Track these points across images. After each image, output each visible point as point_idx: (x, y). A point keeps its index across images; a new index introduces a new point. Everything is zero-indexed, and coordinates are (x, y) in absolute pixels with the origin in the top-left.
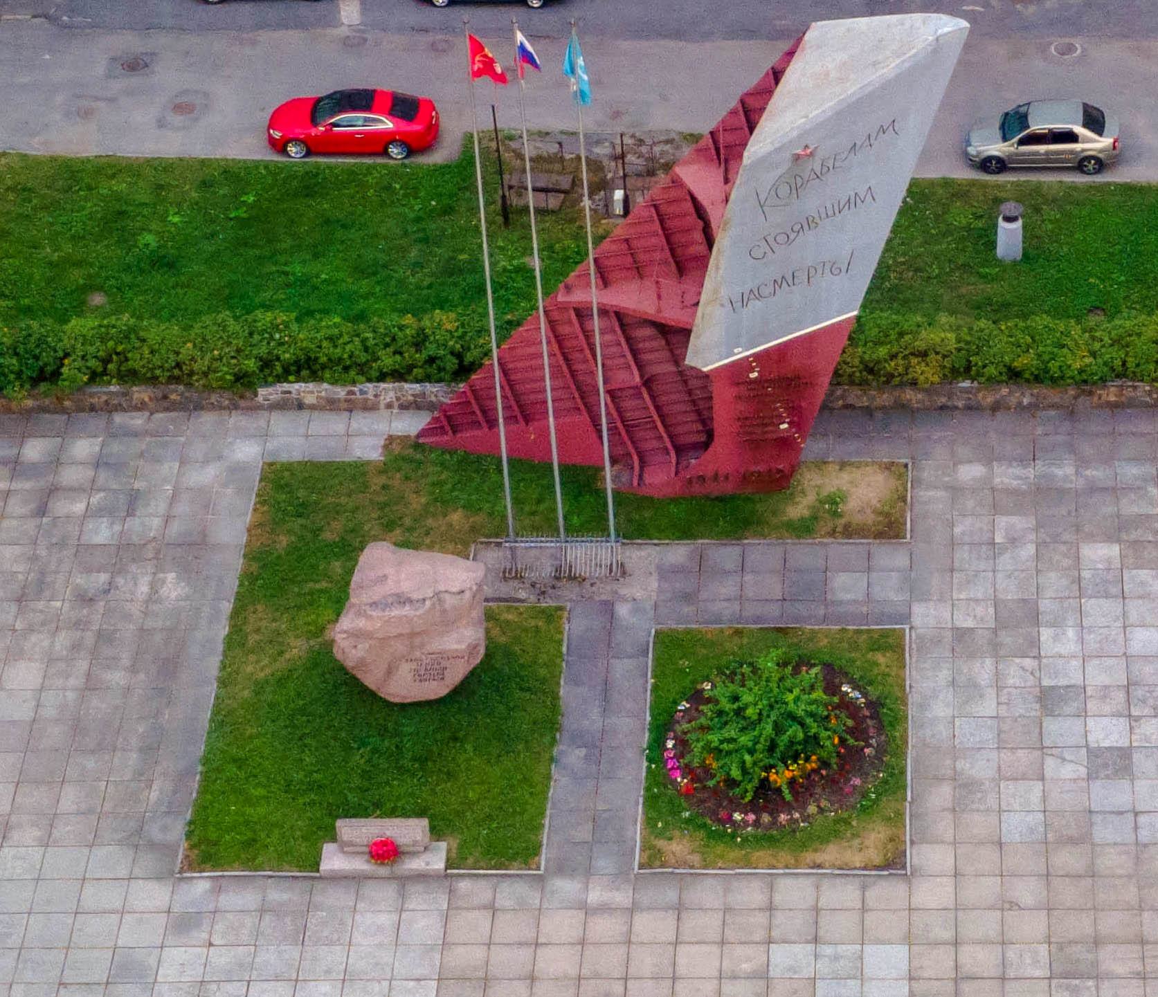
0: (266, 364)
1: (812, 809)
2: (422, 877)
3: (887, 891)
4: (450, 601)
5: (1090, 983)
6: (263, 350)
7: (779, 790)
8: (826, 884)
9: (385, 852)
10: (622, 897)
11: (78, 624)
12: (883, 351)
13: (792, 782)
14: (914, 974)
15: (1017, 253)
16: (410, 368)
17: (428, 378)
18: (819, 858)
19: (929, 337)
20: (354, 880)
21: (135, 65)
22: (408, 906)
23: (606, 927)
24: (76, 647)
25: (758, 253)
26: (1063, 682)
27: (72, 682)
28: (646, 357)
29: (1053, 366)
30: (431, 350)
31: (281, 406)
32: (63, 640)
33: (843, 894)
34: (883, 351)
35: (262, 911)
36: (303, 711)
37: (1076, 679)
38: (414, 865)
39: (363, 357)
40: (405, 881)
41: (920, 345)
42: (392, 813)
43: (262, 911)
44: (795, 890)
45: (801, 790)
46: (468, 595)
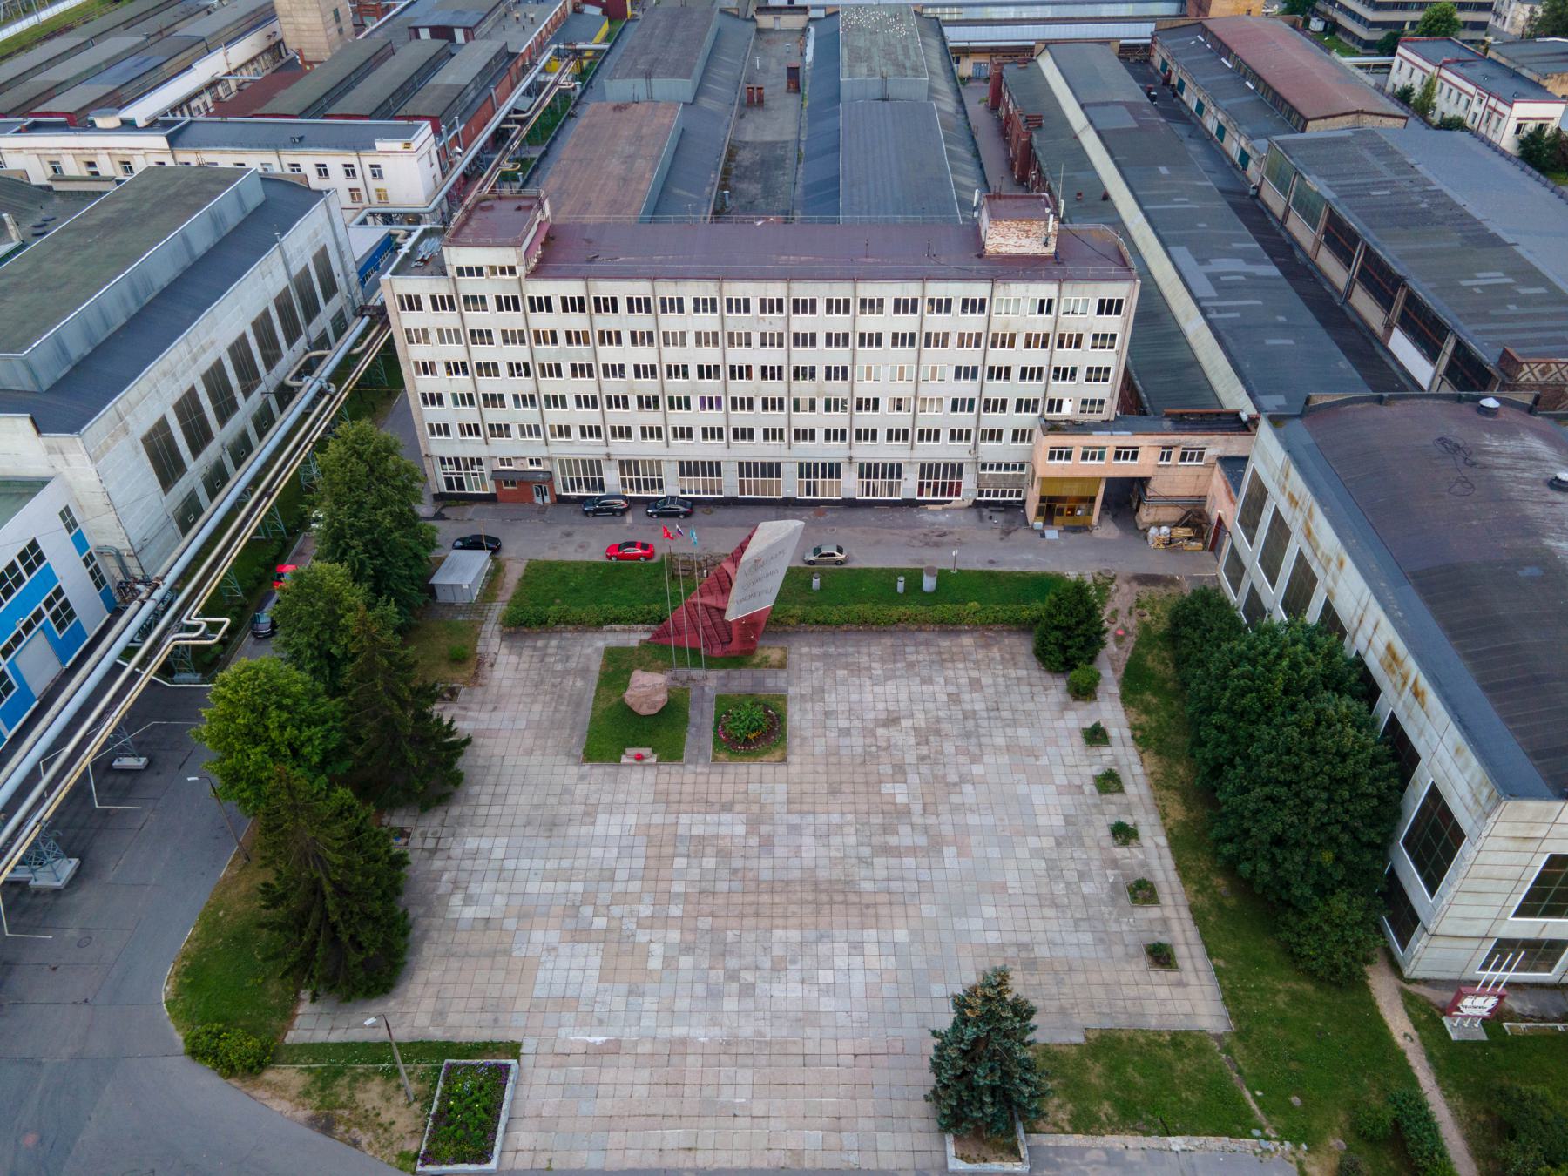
3: (781, 769)
9: (639, 758)
10: (706, 770)
19: (793, 611)
20: (631, 765)
21: (569, 534)
23: (702, 779)
33: (769, 769)
44: (755, 768)
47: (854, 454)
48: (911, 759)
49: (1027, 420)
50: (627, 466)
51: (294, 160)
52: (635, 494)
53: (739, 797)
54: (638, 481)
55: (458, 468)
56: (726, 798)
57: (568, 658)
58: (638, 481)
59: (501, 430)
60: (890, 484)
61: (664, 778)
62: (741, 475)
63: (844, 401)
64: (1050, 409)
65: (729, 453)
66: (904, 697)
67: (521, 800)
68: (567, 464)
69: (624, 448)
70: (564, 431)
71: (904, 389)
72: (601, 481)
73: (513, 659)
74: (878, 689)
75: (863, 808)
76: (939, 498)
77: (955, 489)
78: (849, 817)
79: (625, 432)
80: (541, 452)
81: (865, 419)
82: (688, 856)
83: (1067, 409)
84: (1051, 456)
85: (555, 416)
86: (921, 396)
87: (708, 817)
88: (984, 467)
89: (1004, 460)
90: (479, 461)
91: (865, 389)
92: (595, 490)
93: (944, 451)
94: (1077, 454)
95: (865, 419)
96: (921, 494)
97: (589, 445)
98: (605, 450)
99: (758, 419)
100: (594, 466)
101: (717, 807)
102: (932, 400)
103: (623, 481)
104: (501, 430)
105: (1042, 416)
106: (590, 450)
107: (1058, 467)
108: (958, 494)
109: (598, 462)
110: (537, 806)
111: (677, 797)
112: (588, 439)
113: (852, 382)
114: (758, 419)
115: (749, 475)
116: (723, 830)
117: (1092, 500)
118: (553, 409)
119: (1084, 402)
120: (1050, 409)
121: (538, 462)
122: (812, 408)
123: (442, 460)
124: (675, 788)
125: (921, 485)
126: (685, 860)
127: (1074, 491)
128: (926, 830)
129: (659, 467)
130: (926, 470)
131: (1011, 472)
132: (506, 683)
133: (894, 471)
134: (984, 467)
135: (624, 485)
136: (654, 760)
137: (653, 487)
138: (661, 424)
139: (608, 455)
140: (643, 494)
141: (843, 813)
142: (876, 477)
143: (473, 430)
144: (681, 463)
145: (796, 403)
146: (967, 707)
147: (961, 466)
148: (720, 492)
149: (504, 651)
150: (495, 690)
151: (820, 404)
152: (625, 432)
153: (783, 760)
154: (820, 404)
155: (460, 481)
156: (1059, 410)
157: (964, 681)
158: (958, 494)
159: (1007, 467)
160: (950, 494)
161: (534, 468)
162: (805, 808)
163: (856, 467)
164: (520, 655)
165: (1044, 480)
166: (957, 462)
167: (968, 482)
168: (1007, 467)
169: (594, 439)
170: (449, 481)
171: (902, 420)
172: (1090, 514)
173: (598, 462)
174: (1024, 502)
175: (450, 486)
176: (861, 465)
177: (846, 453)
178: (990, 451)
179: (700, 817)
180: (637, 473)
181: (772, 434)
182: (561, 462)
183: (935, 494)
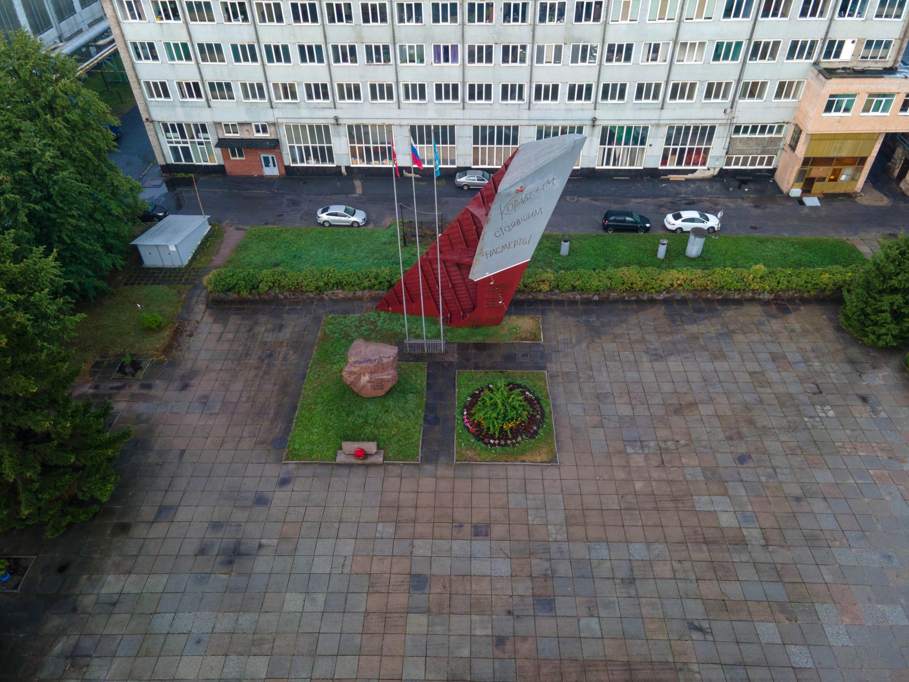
0: (326, 284)
1: (519, 439)
2: (375, 465)
3: (551, 473)
4: (385, 361)
5: (637, 512)
6: (325, 280)
7: (506, 432)
8: (527, 468)
9: (361, 454)
10: (450, 473)
11: (257, 368)
12: (530, 280)
13: (511, 429)
14: (567, 507)
15: (567, 253)
16: (374, 285)
17: (379, 289)
18: (524, 458)
19: (545, 276)
20: (350, 466)
21: (295, 203)
22: (369, 475)
23: (444, 485)
24: (256, 376)
25: (498, 234)
26: (605, 391)
27: (253, 388)
28: (453, 278)
29: (588, 285)
30: (380, 279)
31: (148, 111)
32: (253, 373)
33: (534, 473)
34: (530, 280)
35: (313, 476)
36: (332, 400)
37: (609, 390)
38: (370, 460)
39: (358, 282)
40: (368, 466)
41: (543, 278)
42: (363, 440)
43: (313, 476)
44: (516, 472)
45: (515, 432)
46: (392, 358)
47: (599, 114)
48: (725, 459)
49: (799, 68)
50: (356, 133)
51: (266, 155)
52: (365, 165)
53: (497, 513)
54: (368, 149)
55: (183, 136)
56: (479, 517)
57: (281, 327)
58: (368, 149)
59: (222, 90)
60: (633, 151)
61: (393, 482)
62: (476, 142)
63: (594, 49)
64: (828, 55)
65: (464, 116)
66: (695, 377)
67: (194, 515)
68: (295, 130)
69: (354, 112)
70: (289, 91)
71: (663, 31)
72: (330, 149)
73: (217, 328)
74: (659, 366)
75: (675, 533)
76: (683, 167)
77: (702, 156)
78: (659, 548)
79: (353, 92)
80: (268, 116)
81: (616, 71)
82: (428, 611)
83: (847, 54)
84: (828, 108)
85: (279, 73)
86: (681, 40)
87: (456, 545)
88: (737, 129)
89: (760, 120)
90: (204, 127)
91: (618, 34)
92: (324, 160)
93: (694, 111)
94: (859, 103)
95: (616, 71)
96: (664, 162)
97: (316, 107)
98: (332, 113)
99: (495, 73)
100: (322, 132)
101: (467, 529)
102: (693, 45)
103: (353, 149)
104: (222, 90)
105: (816, 64)
106: (320, 114)
107: (835, 122)
108: (704, 164)
109: (327, 128)
110: (216, 526)
111: (411, 513)
112: (315, 101)
113: (606, 23)
114: (495, 73)
115: (484, 142)
116: (478, 567)
117: (863, 160)
118: (276, 64)
119: (869, 44)
120: (828, 55)
121: (265, 130)
122: (558, 59)
123: (165, 125)
124: (407, 498)
125: (666, 151)
126: (423, 619)
127: (845, 152)
128: (778, 572)
129: (390, 132)
130: (676, 134)
131: (766, 135)
132: (204, 355)
133: (638, 136)
134: (737, 129)
135: (354, 155)
136: (379, 459)
137: (384, 157)
138: (391, 80)
139: (336, 119)
140: (374, 164)
141: (648, 544)
142: (619, 143)
143: (193, 90)
144: (413, 128)
145: (541, 50)
146: (781, 389)
147: (713, 128)
148: (453, 162)
149: (208, 319)
150: (189, 365)
151: (567, 53)
152: (353, 92)
153: (553, 460)
154: (567, 53)
155: (186, 150)
156: (837, 55)
157: (764, 356)
158: (704, 164)
159: (763, 129)
160: (696, 164)
161: (261, 135)
162: (593, 533)
163: (598, 131)
164: (225, 326)
165: (815, 138)
166: (708, 123)
167: (717, 148)
168: (763, 129)
169: (321, 101)
170: (174, 150)
171: (655, 73)
172: (854, 179)
173: (327, 128)
174: (774, 170)
175: (178, 158)
176: (604, 129)
177: (589, 115)
178: (750, 111)
179: (444, 545)
180: (367, 142)
181: (511, 92)
182: (288, 128)
183: (679, 163)
